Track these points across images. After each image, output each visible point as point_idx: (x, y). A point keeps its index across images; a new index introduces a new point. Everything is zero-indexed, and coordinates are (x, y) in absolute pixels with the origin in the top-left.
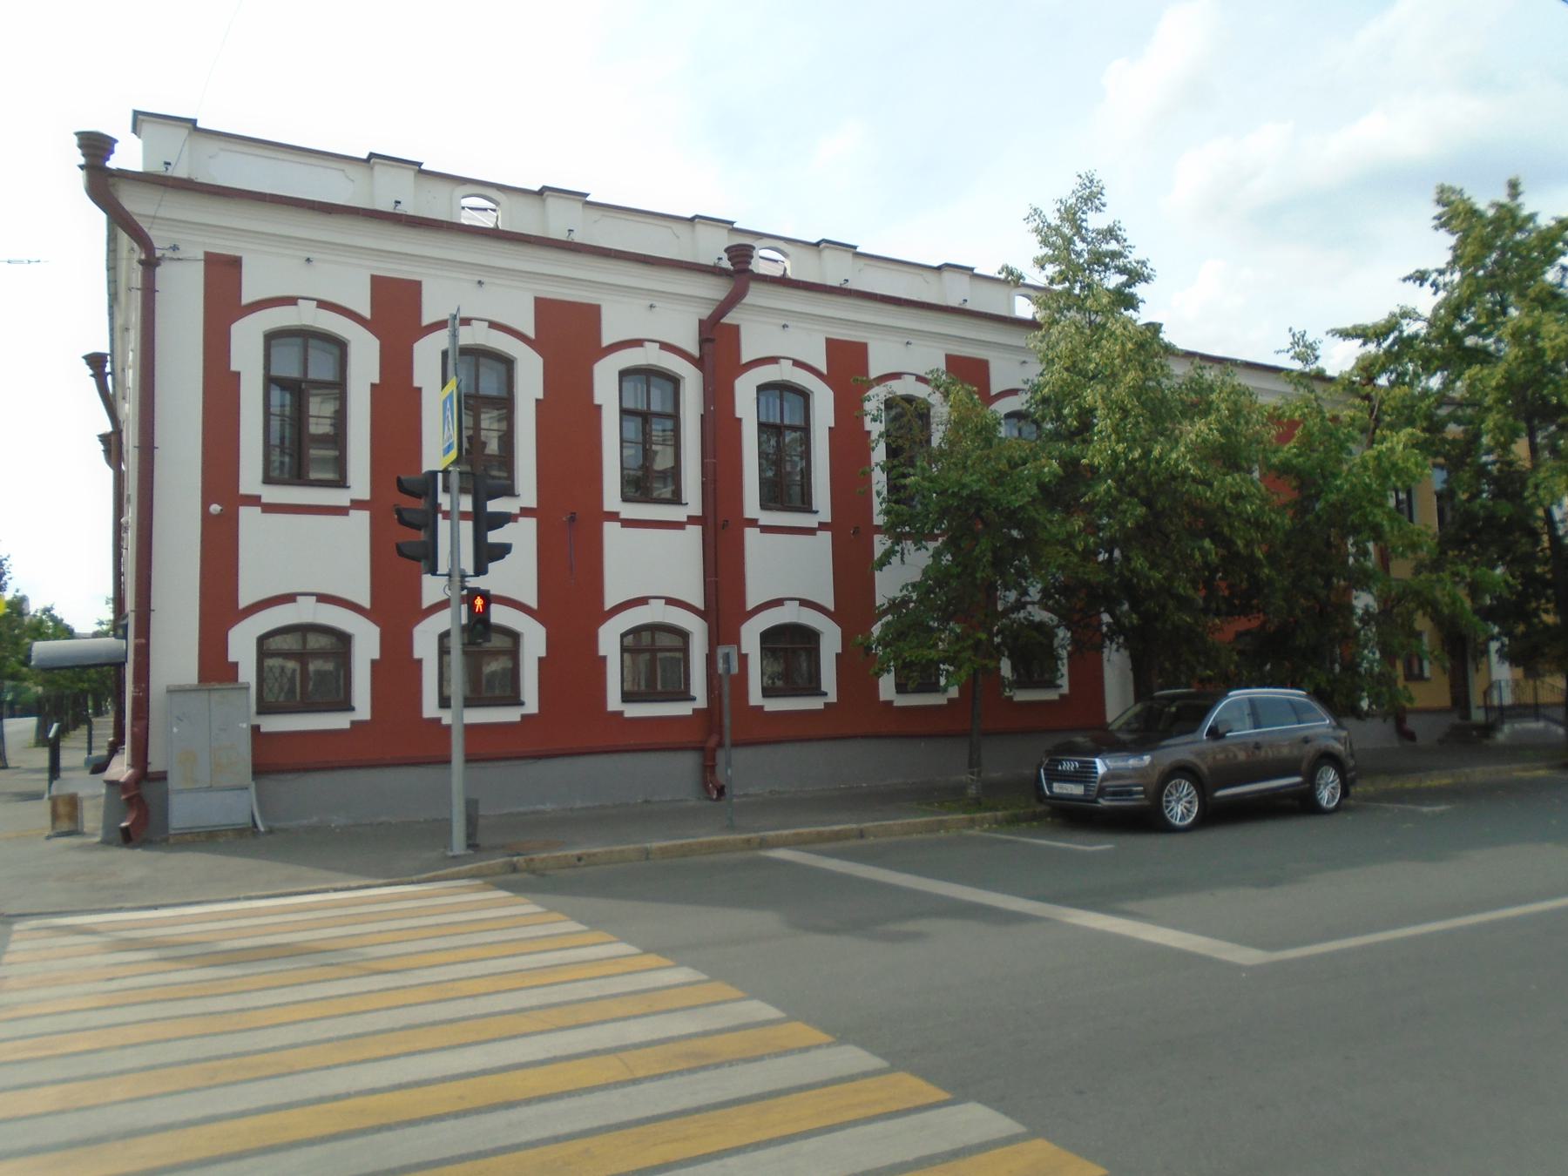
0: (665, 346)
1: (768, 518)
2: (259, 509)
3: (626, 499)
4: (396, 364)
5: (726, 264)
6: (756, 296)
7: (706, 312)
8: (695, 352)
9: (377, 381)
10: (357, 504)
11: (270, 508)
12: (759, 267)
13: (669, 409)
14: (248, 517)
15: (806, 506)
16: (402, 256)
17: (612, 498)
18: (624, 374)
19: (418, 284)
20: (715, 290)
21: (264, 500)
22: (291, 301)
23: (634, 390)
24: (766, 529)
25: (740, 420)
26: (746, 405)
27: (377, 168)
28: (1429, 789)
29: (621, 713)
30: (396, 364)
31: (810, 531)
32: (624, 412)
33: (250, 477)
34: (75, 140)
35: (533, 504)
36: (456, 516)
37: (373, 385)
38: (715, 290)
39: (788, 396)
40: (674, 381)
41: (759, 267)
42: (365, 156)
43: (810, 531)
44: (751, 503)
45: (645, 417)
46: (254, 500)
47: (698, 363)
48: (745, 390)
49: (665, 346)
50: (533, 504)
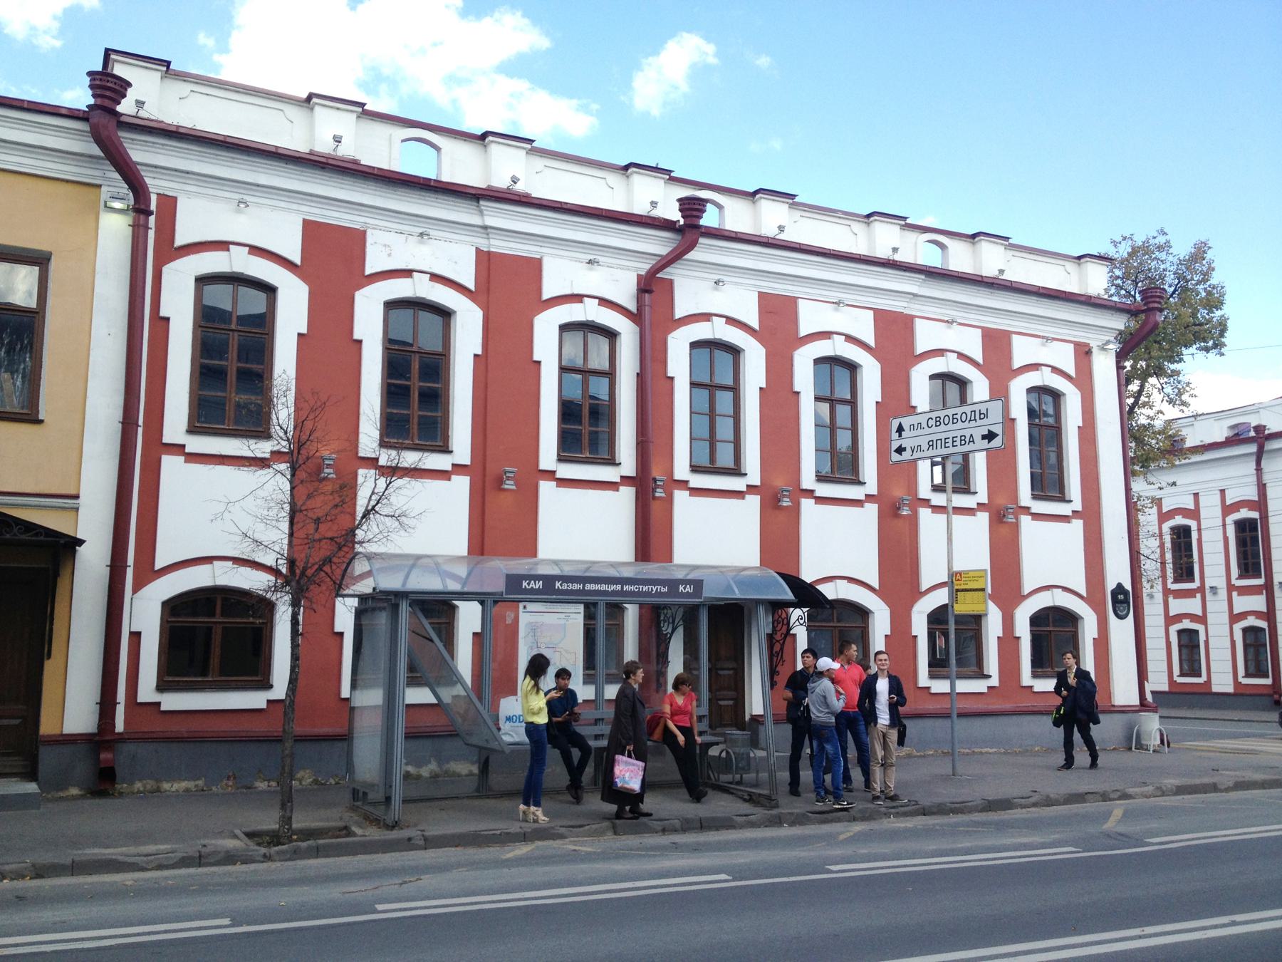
0: (604, 302)
1: (386, 458)
2: (183, 458)
3: (1035, 497)
4: (780, 369)
5: (675, 215)
6: (704, 251)
7: (644, 267)
8: (632, 307)
9: (304, 331)
10: (458, 469)
11: (564, 482)
12: (709, 219)
13: (605, 366)
14: (171, 465)
15: (1062, 498)
16: (342, 203)
17: (548, 455)
18: (565, 328)
19: (175, 199)
20: (657, 244)
21: (558, 475)
22: (223, 245)
23: (404, 323)
24: (696, 492)
25: (1014, 420)
26: (921, 392)
27: (317, 109)
28: (507, 860)
29: (159, 704)
30: (780, 369)
31: (738, 494)
32: (563, 369)
33: (175, 423)
34: (87, 80)
35: (467, 461)
36: (950, 510)
37: (476, 356)
38: (657, 244)
39: (719, 354)
40: (611, 335)
41: (709, 219)
42: (305, 96)
43: (738, 494)
44: (1024, 494)
45: (712, 388)
46: (178, 449)
47: (636, 317)
48: (678, 347)
49: (604, 302)
50: (467, 461)
